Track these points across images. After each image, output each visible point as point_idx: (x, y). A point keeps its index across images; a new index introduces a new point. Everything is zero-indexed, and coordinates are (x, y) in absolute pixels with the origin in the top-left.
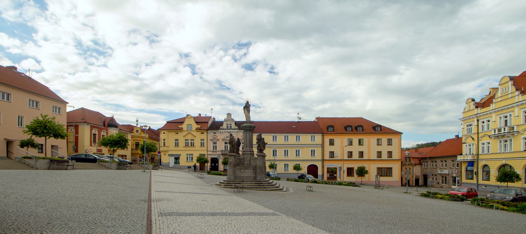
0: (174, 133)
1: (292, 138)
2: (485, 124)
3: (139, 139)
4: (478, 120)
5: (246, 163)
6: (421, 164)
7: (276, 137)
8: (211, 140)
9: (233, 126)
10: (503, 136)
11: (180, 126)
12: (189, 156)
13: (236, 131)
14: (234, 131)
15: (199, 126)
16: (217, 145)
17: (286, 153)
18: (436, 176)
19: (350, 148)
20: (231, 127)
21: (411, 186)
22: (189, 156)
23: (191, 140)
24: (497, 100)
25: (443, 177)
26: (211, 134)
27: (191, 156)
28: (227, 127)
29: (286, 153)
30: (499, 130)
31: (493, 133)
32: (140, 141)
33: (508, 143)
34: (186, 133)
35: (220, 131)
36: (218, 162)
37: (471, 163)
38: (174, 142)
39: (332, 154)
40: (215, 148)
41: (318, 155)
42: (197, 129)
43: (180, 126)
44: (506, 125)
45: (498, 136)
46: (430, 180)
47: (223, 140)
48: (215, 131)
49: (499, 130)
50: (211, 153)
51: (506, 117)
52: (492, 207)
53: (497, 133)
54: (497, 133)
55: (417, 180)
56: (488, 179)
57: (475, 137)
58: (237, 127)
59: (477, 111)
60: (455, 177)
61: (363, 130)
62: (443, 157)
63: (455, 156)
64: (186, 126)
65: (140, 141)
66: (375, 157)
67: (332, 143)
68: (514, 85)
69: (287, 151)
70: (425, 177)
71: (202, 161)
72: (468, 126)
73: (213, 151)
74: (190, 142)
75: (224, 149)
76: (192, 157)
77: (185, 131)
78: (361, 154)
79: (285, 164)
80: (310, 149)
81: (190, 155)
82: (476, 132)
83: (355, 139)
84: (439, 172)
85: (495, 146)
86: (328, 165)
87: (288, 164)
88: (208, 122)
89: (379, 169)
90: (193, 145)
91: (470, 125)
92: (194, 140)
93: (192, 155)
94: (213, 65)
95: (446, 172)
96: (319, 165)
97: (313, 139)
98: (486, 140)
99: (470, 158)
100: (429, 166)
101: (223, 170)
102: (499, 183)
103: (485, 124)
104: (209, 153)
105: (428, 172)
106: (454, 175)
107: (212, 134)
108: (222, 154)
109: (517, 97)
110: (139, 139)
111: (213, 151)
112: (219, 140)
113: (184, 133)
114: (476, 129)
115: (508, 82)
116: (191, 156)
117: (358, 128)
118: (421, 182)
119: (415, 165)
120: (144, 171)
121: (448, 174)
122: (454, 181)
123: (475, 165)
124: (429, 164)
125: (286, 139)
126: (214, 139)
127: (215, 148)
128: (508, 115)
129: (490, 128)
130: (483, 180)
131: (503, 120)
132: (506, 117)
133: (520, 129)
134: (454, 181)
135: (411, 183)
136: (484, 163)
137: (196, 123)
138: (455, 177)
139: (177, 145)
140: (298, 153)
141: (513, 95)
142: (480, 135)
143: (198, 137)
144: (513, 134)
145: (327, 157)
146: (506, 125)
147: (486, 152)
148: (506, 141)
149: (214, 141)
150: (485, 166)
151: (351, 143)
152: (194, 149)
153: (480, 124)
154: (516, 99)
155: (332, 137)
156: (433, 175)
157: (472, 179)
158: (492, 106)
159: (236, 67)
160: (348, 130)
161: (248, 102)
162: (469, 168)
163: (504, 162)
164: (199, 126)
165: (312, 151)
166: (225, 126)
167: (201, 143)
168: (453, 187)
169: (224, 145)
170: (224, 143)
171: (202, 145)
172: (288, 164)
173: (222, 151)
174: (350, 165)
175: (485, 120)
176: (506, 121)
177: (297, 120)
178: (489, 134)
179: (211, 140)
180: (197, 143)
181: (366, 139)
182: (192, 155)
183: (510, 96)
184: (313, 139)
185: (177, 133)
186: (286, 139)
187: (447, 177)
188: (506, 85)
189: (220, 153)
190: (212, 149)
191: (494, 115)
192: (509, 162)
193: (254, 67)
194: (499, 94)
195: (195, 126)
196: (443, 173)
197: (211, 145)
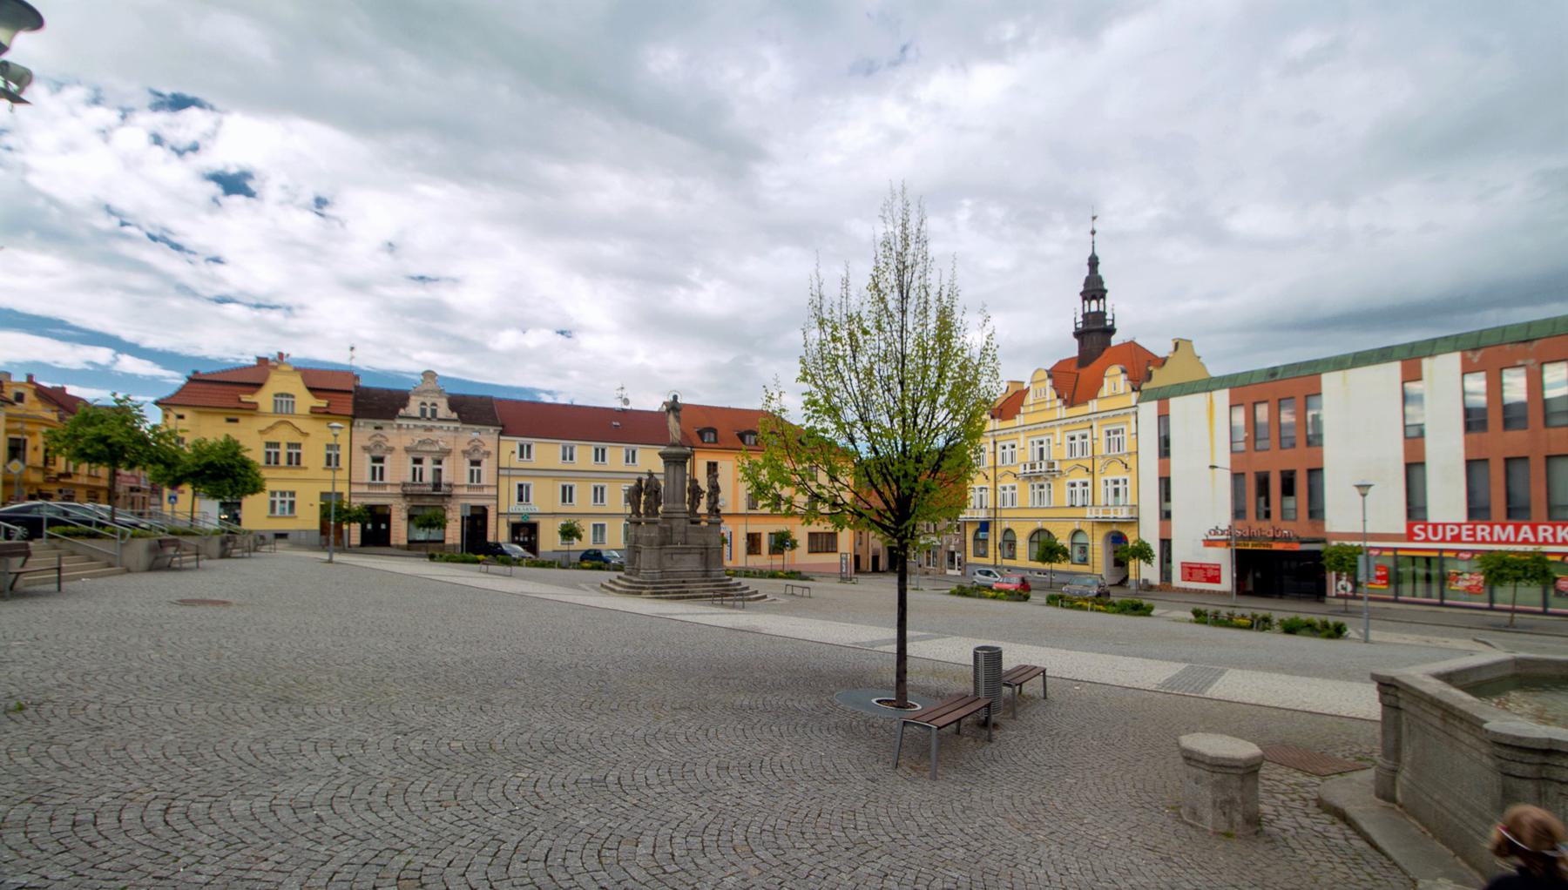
0: (221, 420)
1: (584, 453)
3: (28, 428)
5: (676, 537)
7: (529, 447)
8: (365, 449)
9: (443, 410)
11: (245, 398)
12: (278, 498)
13: (452, 425)
14: (445, 425)
15: (323, 403)
16: (387, 465)
17: (599, 494)
20: (434, 412)
21: (865, 573)
22: (278, 498)
23: (290, 445)
26: (365, 431)
27: (288, 499)
28: (423, 412)
29: (599, 494)
30: (1033, 466)
32: (32, 434)
33: (1045, 490)
34: (271, 421)
35: (399, 421)
36: (387, 519)
37: (984, 526)
38: (323, 452)
40: (377, 473)
42: (314, 411)
43: (245, 398)
44: (1041, 458)
47: (408, 450)
48: (379, 422)
49: (1033, 466)
50: (365, 489)
52: (1080, 608)
55: (876, 559)
56: (1013, 557)
60: (953, 553)
64: (271, 399)
65: (32, 434)
68: (1054, 386)
71: (334, 516)
73: (370, 485)
74: (283, 452)
75: (409, 479)
76: (292, 504)
77: (265, 415)
80: (592, 485)
81: (283, 494)
85: (1025, 494)
87: (603, 526)
89: (812, 535)
90: (295, 460)
91: (1116, 432)
92: (298, 446)
93: (293, 494)
94: (70, 146)
98: (1008, 482)
99: (982, 515)
101: (404, 542)
102: (1039, 565)
103: (1008, 450)
104: (355, 489)
106: (952, 548)
107: (370, 431)
108: (405, 495)
110: (28, 428)
111: (370, 485)
112: (391, 450)
113: (263, 423)
116: (288, 499)
120: (330, 561)
122: (952, 560)
123: (992, 529)
125: (600, 455)
126: (378, 445)
127: (377, 473)
128: (1044, 439)
129: (1017, 460)
131: (1037, 447)
133: (1065, 467)
134: (952, 560)
135: (863, 565)
136: (1006, 525)
137: (312, 390)
138: (953, 553)
142: (999, 471)
143: (317, 438)
146: (1041, 458)
147: (1009, 505)
148: (1042, 487)
149: (378, 453)
150: (1008, 530)
152: (301, 474)
153: (999, 451)
155: (713, 458)
157: (985, 555)
158: (1019, 420)
159: (179, 174)
162: (981, 535)
163: (1039, 525)
164: (323, 403)
166: (413, 408)
167: (329, 456)
168: (949, 572)
169: (410, 465)
170: (410, 461)
171: (331, 461)
172: (603, 526)
173: (404, 485)
174: (753, 528)
175: (1007, 444)
176: (1041, 450)
177: (618, 405)
179: (365, 449)
180: (313, 455)
182: (293, 494)
183: (1048, 405)
185: (236, 421)
186: (600, 455)
189: (398, 490)
190: (368, 479)
191: (1022, 436)
194: (1030, 399)
195: (305, 401)
197: (364, 466)
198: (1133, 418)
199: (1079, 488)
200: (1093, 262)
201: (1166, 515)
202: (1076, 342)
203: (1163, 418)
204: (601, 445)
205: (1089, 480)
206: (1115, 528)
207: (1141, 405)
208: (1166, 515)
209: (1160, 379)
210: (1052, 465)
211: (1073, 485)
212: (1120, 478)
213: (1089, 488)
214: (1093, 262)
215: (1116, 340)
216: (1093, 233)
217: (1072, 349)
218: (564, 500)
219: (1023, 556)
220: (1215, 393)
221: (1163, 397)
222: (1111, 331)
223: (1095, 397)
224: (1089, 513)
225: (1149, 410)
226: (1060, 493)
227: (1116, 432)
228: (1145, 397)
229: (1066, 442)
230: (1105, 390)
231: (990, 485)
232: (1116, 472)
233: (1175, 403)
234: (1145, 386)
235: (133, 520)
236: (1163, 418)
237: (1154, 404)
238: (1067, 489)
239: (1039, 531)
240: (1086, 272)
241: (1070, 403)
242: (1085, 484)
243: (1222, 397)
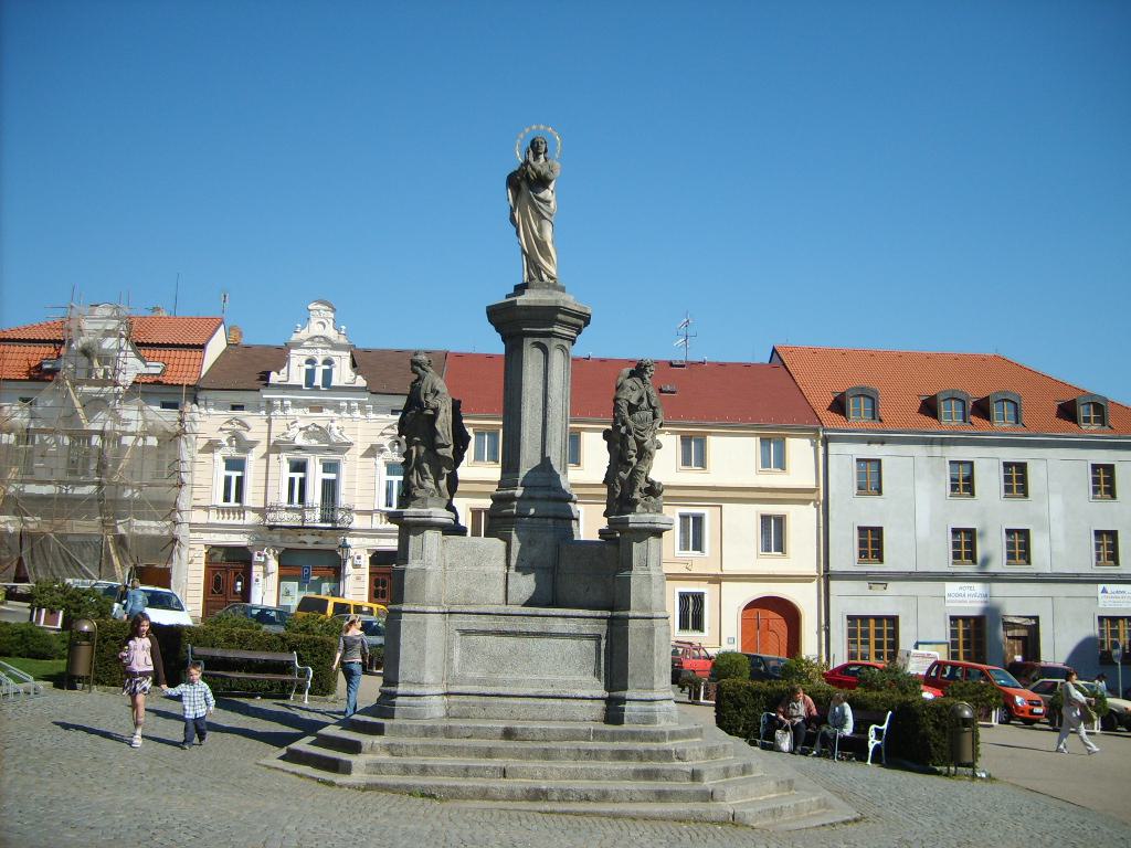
13: (354, 399)
19: (1015, 514)
20: (327, 375)
28: (310, 375)
39: (871, 541)
40: (235, 489)
41: (801, 553)
48: (237, 398)
50: (214, 518)
58: (361, 382)
66: (1085, 562)
67: (871, 479)
78: (1019, 543)
79: (765, 519)
83: (988, 465)
86: (852, 599)
88: (202, 347)
96: (804, 598)
127: (235, 489)
145: (845, 555)
151: (964, 483)
155: (1103, 457)
181: (1046, 466)
193: (540, 164)
204: (1103, 457)
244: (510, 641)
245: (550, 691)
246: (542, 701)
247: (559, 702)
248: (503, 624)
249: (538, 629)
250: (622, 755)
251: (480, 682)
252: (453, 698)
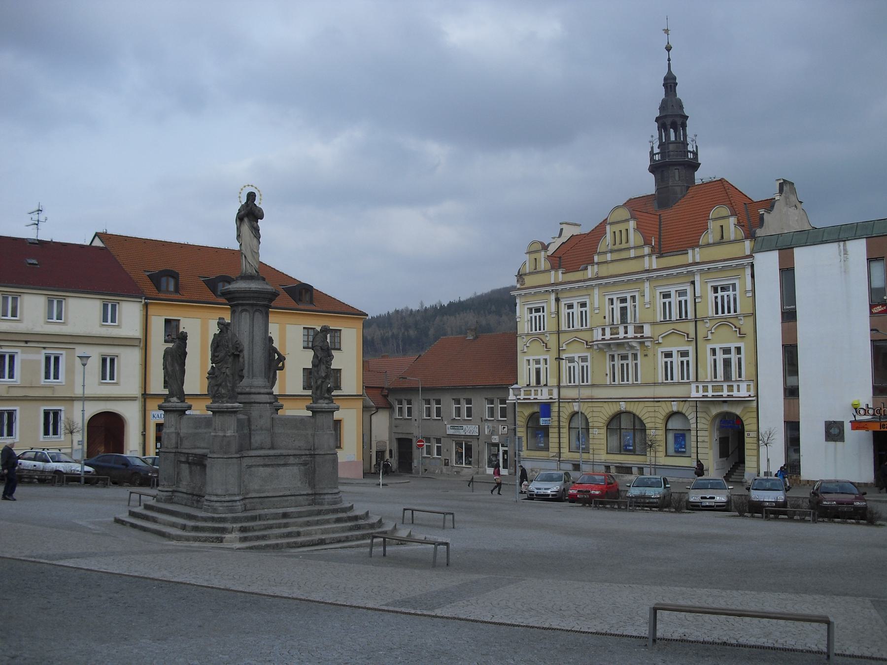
2: (577, 310)
4: (557, 300)
6: (390, 407)
10: (619, 345)
18: (438, 441)
24: (602, 258)
25: (459, 445)
31: (600, 337)
33: (630, 361)
45: (609, 345)
46: (418, 456)
51: (624, 300)
53: (608, 336)
54: (608, 336)
57: (552, 340)
59: (556, 277)
61: (177, 290)
62: (464, 389)
63: (505, 389)
69: (57, 359)
70: (405, 446)
72: (531, 310)
82: (555, 329)
84: (450, 432)
85: (600, 368)
91: (538, 310)
95: (471, 429)
97: (109, 315)
100: (415, 413)
103: (577, 310)
105: (415, 431)
106: (495, 439)
109: (647, 258)
114: (555, 321)
115: (627, 220)
117: (164, 279)
118: (394, 463)
119: (377, 408)
121: (477, 438)
124: (415, 407)
130: (666, 455)
131: (617, 305)
132: (624, 300)
139: (546, 360)
140: (52, 366)
141: (639, 252)
144: (644, 343)
153: (564, 311)
154: (646, 263)
156: (428, 440)
160: (163, 287)
161: (251, 196)
163: (623, 406)
165: (104, 360)
176: (624, 310)
178: (586, 336)
183: (632, 253)
184: (109, 315)
187: (474, 444)
188: (622, 227)
192: (638, 409)
196: (462, 432)
198: (748, 271)
199: (676, 359)
200: (670, 83)
201: (791, 392)
202: (652, 177)
203: (787, 273)
205: (691, 349)
206: (726, 408)
207: (756, 255)
208: (791, 392)
209: (773, 224)
210: (639, 329)
211: (669, 355)
212: (733, 346)
213: (691, 358)
214: (670, 83)
215: (700, 176)
216: (668, 49)
217: (648, 185)
218: (46, 433)
219: (601, 450)
220: (849, 244)
221: (785, 247)
222: (694, 165)
223: (695, 245)
224: (695, 393)
225: (768, 264)
226: (651, 366)
227: (538, 310)
228: (763, 246)
229: (660, 301)
230: (711, 236)
231: (551, 357)
232: (725, 339)
233: (802, 256)
234: (759, 232)
235: (351, 381)
236: (787, 273)
237: (775, 254)
238: (661, 360)
239: (617, 416)
240: (661, 94)
241: (660, 252)
242: (684, 354)
243: (858, 249)
244: (269, 470)
245: (288, 493)
246: (286, 498)
247: (293, 498)
248: (267, 461)
249: (282, 462)
250: (338, 520)
251: (258, 491)
252: (247, 501)
